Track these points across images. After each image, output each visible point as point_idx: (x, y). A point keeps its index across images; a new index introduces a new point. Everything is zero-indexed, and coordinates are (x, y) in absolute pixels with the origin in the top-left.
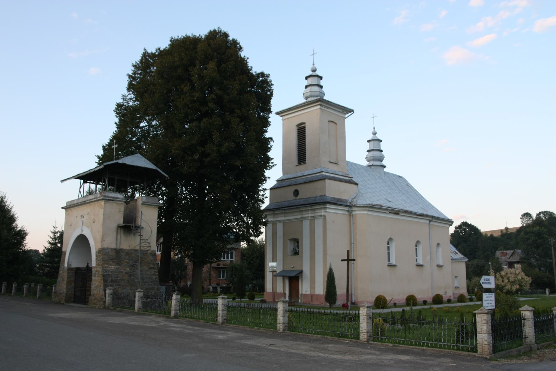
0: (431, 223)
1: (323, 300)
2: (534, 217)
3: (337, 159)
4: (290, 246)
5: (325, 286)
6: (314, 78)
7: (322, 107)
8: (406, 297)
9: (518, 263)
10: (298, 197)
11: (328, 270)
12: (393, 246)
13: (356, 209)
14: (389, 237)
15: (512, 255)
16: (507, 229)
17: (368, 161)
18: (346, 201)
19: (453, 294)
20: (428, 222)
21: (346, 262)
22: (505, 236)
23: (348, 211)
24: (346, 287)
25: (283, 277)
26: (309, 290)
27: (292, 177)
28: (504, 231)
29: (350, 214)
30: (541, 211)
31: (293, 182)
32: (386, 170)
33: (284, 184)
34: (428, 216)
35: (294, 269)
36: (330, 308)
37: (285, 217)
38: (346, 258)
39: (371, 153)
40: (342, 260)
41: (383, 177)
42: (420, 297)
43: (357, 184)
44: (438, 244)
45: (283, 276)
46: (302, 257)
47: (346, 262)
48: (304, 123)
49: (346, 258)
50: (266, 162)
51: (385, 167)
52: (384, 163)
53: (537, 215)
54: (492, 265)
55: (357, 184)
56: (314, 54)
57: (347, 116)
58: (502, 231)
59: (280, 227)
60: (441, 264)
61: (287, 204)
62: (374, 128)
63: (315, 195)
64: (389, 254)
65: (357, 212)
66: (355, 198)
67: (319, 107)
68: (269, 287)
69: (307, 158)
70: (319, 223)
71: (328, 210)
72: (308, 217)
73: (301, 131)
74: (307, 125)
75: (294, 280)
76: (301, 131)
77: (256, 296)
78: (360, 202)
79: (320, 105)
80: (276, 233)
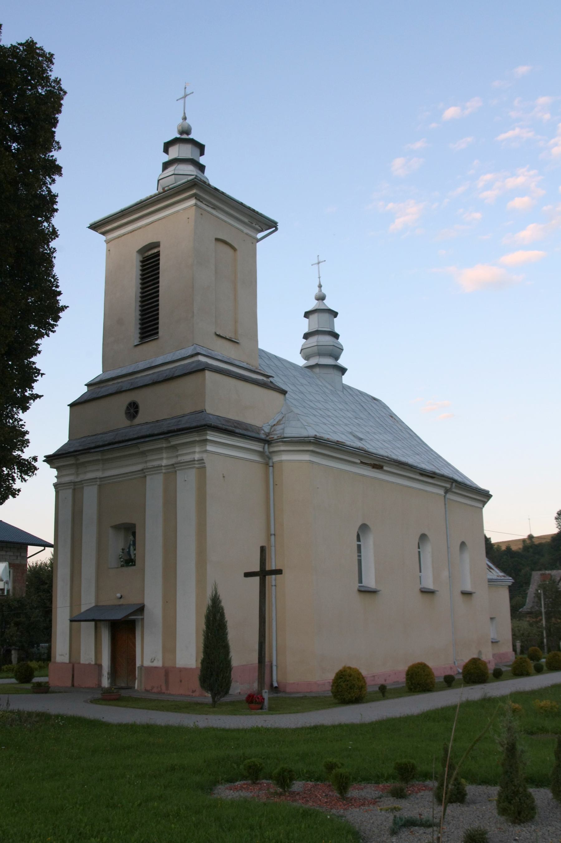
0: (449, 496)
1: (196, 683)
3: (236, 332)
4: (116, 545)
5: (201, 646)
6: (185, 146)
7: (199, 203)
13: (282, 448)
14: (360, 523)
16: (531, 537)
17: (307, 358)
19: (494, 655)
20: (442, 492)
21: (257, 579)
23: (261, 454)
24: (257, 647)
26: (160, 656)
27: (124, 372)
29: (267, 460)
31: (125, 383)
32: (347, 379)
33: (104, 390)
35: (122, 602)
36: (214, 704)
37: (104, 470)
38: (257, 569)
39: (313, 341)
40: (247, 575)
41: (340, 393)
42: (441, 663)
43: (284, 392)
44: (463, 544)
46: (143, 570)
47: (257, 579)
48: (157, 245)
49: (257, 569)
50: (46, 309)
51: (343, 370)
52: (342, 362)
54: (545, 594)
56: (185, 96)
58: (524, 541)
59: (90, 495)
60: (468, 588)
61: (109, 438)
62: (320, 286)
65: (285, 457)
66: (278, 423)
67: (193, 201)
68: (61, 650)
69: (161, 325)
70: (186, 481)
71: (209, 448)
72: (160, 466)
73: (150, 264)
74: (162, 249)
75: (123, 629)
76: (150, 264)
77: (36, 673)
78: (291, 431)
79: (195, 196)
80: (81, 512)
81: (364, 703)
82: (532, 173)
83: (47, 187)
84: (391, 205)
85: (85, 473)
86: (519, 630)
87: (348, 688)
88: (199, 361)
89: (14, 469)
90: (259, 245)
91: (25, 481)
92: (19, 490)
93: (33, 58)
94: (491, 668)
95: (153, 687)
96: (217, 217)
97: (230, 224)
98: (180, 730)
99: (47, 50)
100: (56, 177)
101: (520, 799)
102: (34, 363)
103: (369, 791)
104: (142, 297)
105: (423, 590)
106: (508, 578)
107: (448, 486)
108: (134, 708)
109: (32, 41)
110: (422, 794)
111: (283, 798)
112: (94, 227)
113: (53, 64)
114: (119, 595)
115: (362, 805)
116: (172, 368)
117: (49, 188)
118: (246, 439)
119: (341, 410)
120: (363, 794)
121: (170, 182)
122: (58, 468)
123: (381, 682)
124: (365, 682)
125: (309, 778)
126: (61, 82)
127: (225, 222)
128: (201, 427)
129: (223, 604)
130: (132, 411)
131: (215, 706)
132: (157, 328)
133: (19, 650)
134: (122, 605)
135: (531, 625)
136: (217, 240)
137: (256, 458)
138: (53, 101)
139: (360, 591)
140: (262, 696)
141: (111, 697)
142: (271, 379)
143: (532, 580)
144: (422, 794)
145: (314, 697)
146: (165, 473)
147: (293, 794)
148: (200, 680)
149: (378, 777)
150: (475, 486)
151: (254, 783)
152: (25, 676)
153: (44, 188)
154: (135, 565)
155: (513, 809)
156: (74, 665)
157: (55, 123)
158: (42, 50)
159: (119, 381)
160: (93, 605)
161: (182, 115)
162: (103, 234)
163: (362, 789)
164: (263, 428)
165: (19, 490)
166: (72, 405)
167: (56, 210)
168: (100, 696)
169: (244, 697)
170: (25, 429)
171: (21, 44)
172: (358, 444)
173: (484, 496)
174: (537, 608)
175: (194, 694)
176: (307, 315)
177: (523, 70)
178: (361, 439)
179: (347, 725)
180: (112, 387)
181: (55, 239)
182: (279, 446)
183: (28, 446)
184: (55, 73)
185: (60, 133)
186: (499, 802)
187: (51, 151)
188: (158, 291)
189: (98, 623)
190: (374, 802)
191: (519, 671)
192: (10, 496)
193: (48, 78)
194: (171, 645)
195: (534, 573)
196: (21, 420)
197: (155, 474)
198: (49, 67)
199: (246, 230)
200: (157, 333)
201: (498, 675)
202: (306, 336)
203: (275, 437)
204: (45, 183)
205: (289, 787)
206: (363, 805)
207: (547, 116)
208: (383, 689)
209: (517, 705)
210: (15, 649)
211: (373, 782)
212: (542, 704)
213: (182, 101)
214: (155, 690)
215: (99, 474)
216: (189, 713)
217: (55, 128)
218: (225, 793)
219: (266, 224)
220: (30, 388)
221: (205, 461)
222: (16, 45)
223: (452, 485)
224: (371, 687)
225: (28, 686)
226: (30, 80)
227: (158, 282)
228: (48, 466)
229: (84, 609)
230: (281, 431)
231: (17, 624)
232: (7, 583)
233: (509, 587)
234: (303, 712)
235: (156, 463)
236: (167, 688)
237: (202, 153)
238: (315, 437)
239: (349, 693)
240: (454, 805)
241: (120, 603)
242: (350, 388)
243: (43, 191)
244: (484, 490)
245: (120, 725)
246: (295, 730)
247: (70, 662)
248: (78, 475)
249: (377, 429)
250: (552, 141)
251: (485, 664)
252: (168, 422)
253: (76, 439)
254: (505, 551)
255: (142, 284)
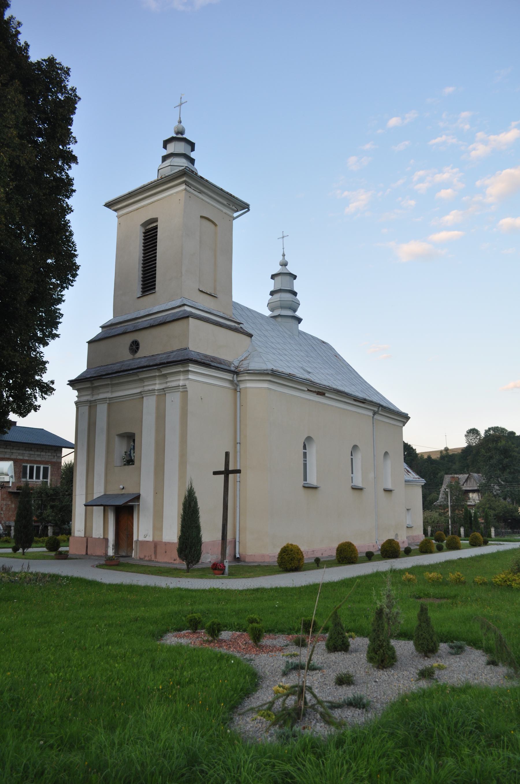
0: (376, 417)
2: (482, 434)
3: (215, 289)
4: (120, 448)
7: (188, 188)
8: (336, 545)
9: (473, 491)
10: (139, 354)
11: (185, 493)
12: (313, 452)
15: (466, 481)
16: (446, 449)
17: (272, 310)
18: (230, 364)
19: (407, 538)
20: (371, 414)
21: (222, 477)
22: (446, 459)
23: (231, 382)
25: (105, 507)
28: (444, 452)
29: (235, 386)
30: (490, 426)
31: (130, 326)
32: (302, 327)
34: (372, 403)
35: (123, 492)
36: (188, 570)
37: (112, 392)
38: (223, 469)
39: (277, 297)
40: (215, 473)
41: (297, 338)
42: (363, 544)
43: (251, 336)
44: (386, 453)
45: (105, 506)
46: (139, 468)
47: (222, 477)
48: (155, 220)
49: (223, 469)
50: (66, 269)
51: (299, 320)
52: (298, 314)
53: (486, 431)
54: (451, 492)
55: (251, 336)
57: (235, 215)
58: (441, 452)
59: (102, 410)
60: (389, 487)
61: (116, 368)
62: (284, 255)
63: (170, 350)
64: (305, 465)
65: (249, 385)
66: (245, 359)
67: (183, 187)
68: (78, 526)
70: (173, 401)
71: (191, 376)
73: (150, 235)
75: (124, 512)
76: (150, 235)
77: (61, 545)
78: (255, 365)
79: (185, 182)
81: (301, 571)
82: (455, 170)
83: (66, 173)
84: (346, 193)
85: (98, 394)
86: (431, 519)
87: (290, 560)
88: (185, 310)
89: (36, 390)
90: (234, 222)
91: (45, 399)
92: (39, 406)
93: (53, 71)
94: (402, 547)
95: (145, 556)
96: (202, 199)
97: (212, 205)
98: (155, 589)
99: (65, 64)
100: (73, 165)
101: (383, 651)
102: (59, 309)
103: (281, 640)
104: (143, 260)
105: (354, 487)
106: (421, 479)
107: (376, 409)
108: (127, 572)
109: (53, 58)
110: (319, 643)
111: (212, 644)
112: (109, 205)
113: (70, 76)
114: (121, 487)
115: (270, 651)
116: (165, 315)
117: (67, 173)
118: (219, 370)
119: (296, 350)
120: (275, 643)
121: (168, 172)
122: (78, 390)
123: (318, 555)
124: (302, 555)
125: (239, 629)
126: (77, 91)
127: (208, 203)
128: (184, 360)
129: (196, 495)
130: (134, 347)
131: (189, 572)
132: (155, 284)
133: (53, 526)
134: (124, 494)
135: (440, 515)
136: (202, 217)
137: (227, 385)
138: (70, 103)
139: (304, 487)
140: (223, 564)
141: (111, 564)
142: (241, 325)
143: (444, 482)
144: (319, 643)
145: (265, 566)
146: (157, 395)
147: (221, 641)
148: (178, 551)
149: (291, 629)
150: (397, 410)
151: (194, 632)
152: (53, 546)
153: (63, 174)
154: (134, 464)
155: (377, 658)
156: (87, 538)
157: (70, 122)
158: (61, 65)
159: (126, 324)
160: (103, 494)
161: (178, 119)
162: (115, 210)
163: (275, 639)
164: (234, 362)
165: (39, 406)
166: (89, 342)
167: (75, 191)
168: (104, 562)
169: (210, 565)
170: (44, 359)
171: (44, 60)
172: (307, 376)
173: (404, 418)
174: (445, 503)
175: (175, 562)
176: (273, 277)
177: (449, 90)
178: (309, 373)
179: (281, 589)
180: (119, 329)
181: (70, 213)
182: (245, 376)
183: (46, 372)
184: (71, 83)
185: (76, 129)
186: (368, 652)
187: (70, 144)
188: (156, 256)
189: (106, 507)
190: (281, 649)
191: (425, 549)
192: (33, 411)
193: (65, 87)
194: (158, 527)
195: (446, 476)
196: (42, 353)
197: (150, 395)
198: (66, 79)
199: (225, 210)
200: (155, 288)
201: (408, 552)
202: (272, 293)
203: (242, 369)
204: (63, 170)
205: (217, 636)
206: (271, 651)
207: (467, 127)
208: (317, 560)
209: (411, 576)
210: (51, 526)
211: (286, 633)
212: (431, 576)
213: (178, 108)
214: (147, 558)
215: (109, 395)
216: (167, 576)
217: (71, 126)
218: (171, 640)
219: (241, 206)
220: (55, 328)
221: (187, 387)
222: (41, 61)
223: (379, 409)
224: (308, 558)
225: (53, 554)
226: (51, 89)
227: (156, 249)
228: (71, 388)
229: (96, 496)
230: (247, 365)
231: (52, 507)
232: (12, 477)
233: (422, 486)
234: (253, 577)
235: (151, 388)
236: (156, 557)
237: (193, 150)
238: (272, 370)
239: (291, 564)
240: (340, 653)
241: (122, 493)
242: (304, 333)
243: (63, 175)
244: (404, 413)
245: (110, 585)
246: (241, 592)
247: (85, 537)
248: (93, 395)
249: (323, 365)
250: (471, 146)
251: (398, 544)
252: (161, 356)
253: (92, 368)
254: (426, 459)
255: (144, 250)
